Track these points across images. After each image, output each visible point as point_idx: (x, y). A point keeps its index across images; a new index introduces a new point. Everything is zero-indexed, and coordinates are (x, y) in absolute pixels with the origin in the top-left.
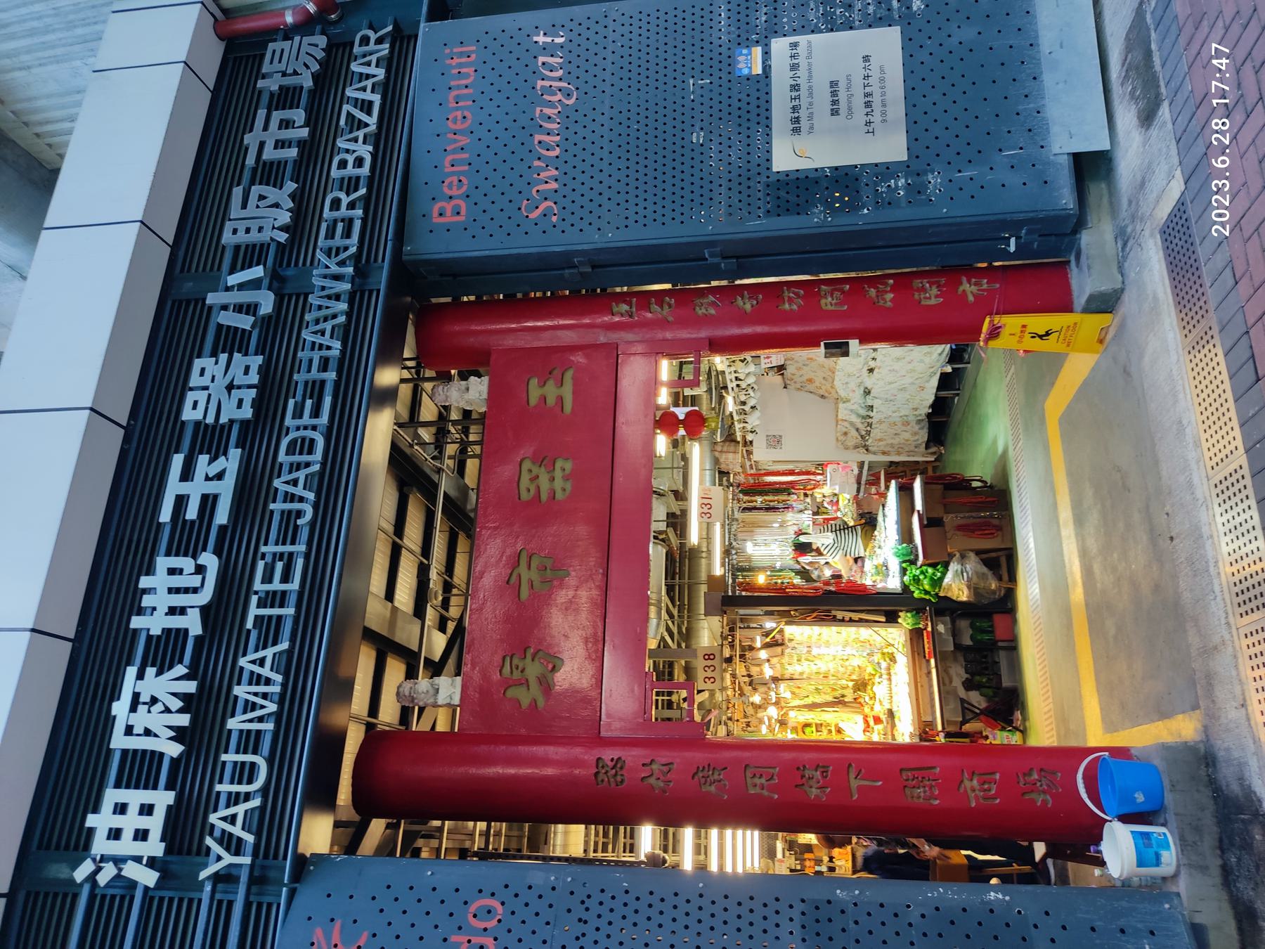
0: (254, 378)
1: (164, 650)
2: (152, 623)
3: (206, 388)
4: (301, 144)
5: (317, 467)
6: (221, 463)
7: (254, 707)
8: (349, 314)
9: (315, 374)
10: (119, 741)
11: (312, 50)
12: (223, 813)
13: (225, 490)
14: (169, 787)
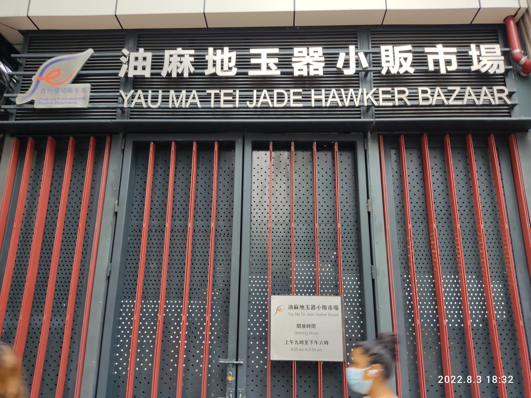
0: (312, 73)
1: (465, 60)
2: (473, 51)
3: (308, 54)
4: (437, 71)
5: (271, 105)
6: (274, 67)
7: (177, 98)
8: (344, 107)
9: (313, 97)
10: (167, 53)
11: (495, 66)
12: (488, 91)
13: (263, 72)
14: (152, 74)
